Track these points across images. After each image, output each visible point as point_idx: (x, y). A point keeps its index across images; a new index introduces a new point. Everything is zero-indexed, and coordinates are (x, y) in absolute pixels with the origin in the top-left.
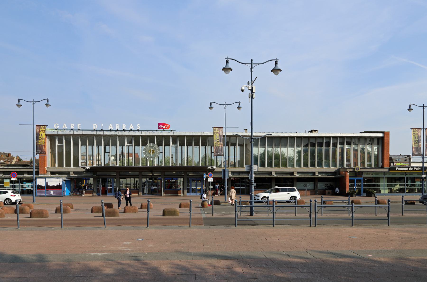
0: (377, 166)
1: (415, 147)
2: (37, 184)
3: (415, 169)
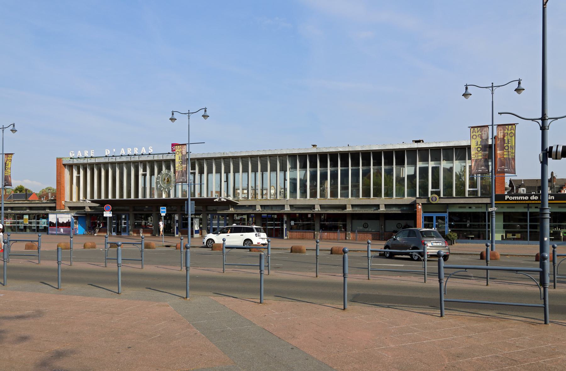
1: (476, 158)
2: (49, 221)
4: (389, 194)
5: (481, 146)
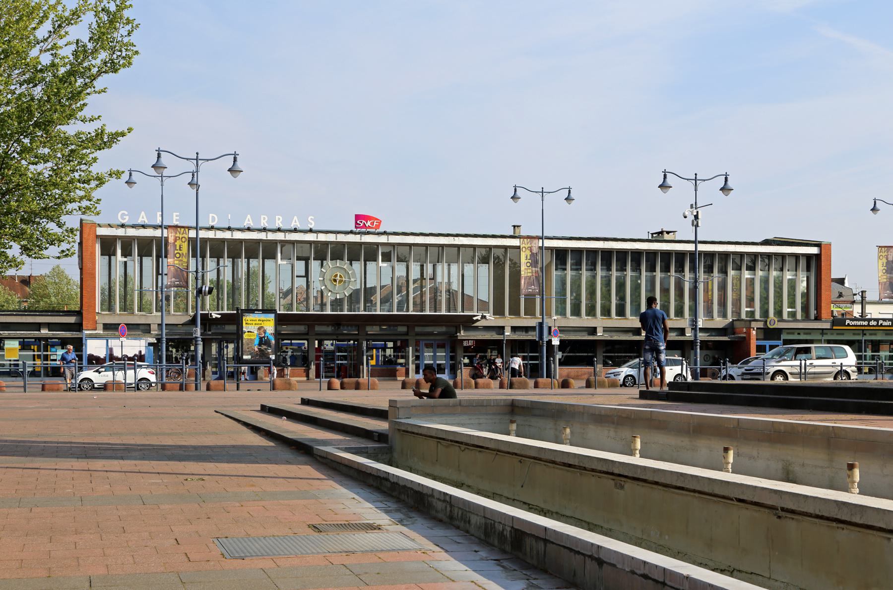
0: (806, 317)
1: (526, 275)
3: (881, 324)
4: (606, 312)
5: (886, 268)
